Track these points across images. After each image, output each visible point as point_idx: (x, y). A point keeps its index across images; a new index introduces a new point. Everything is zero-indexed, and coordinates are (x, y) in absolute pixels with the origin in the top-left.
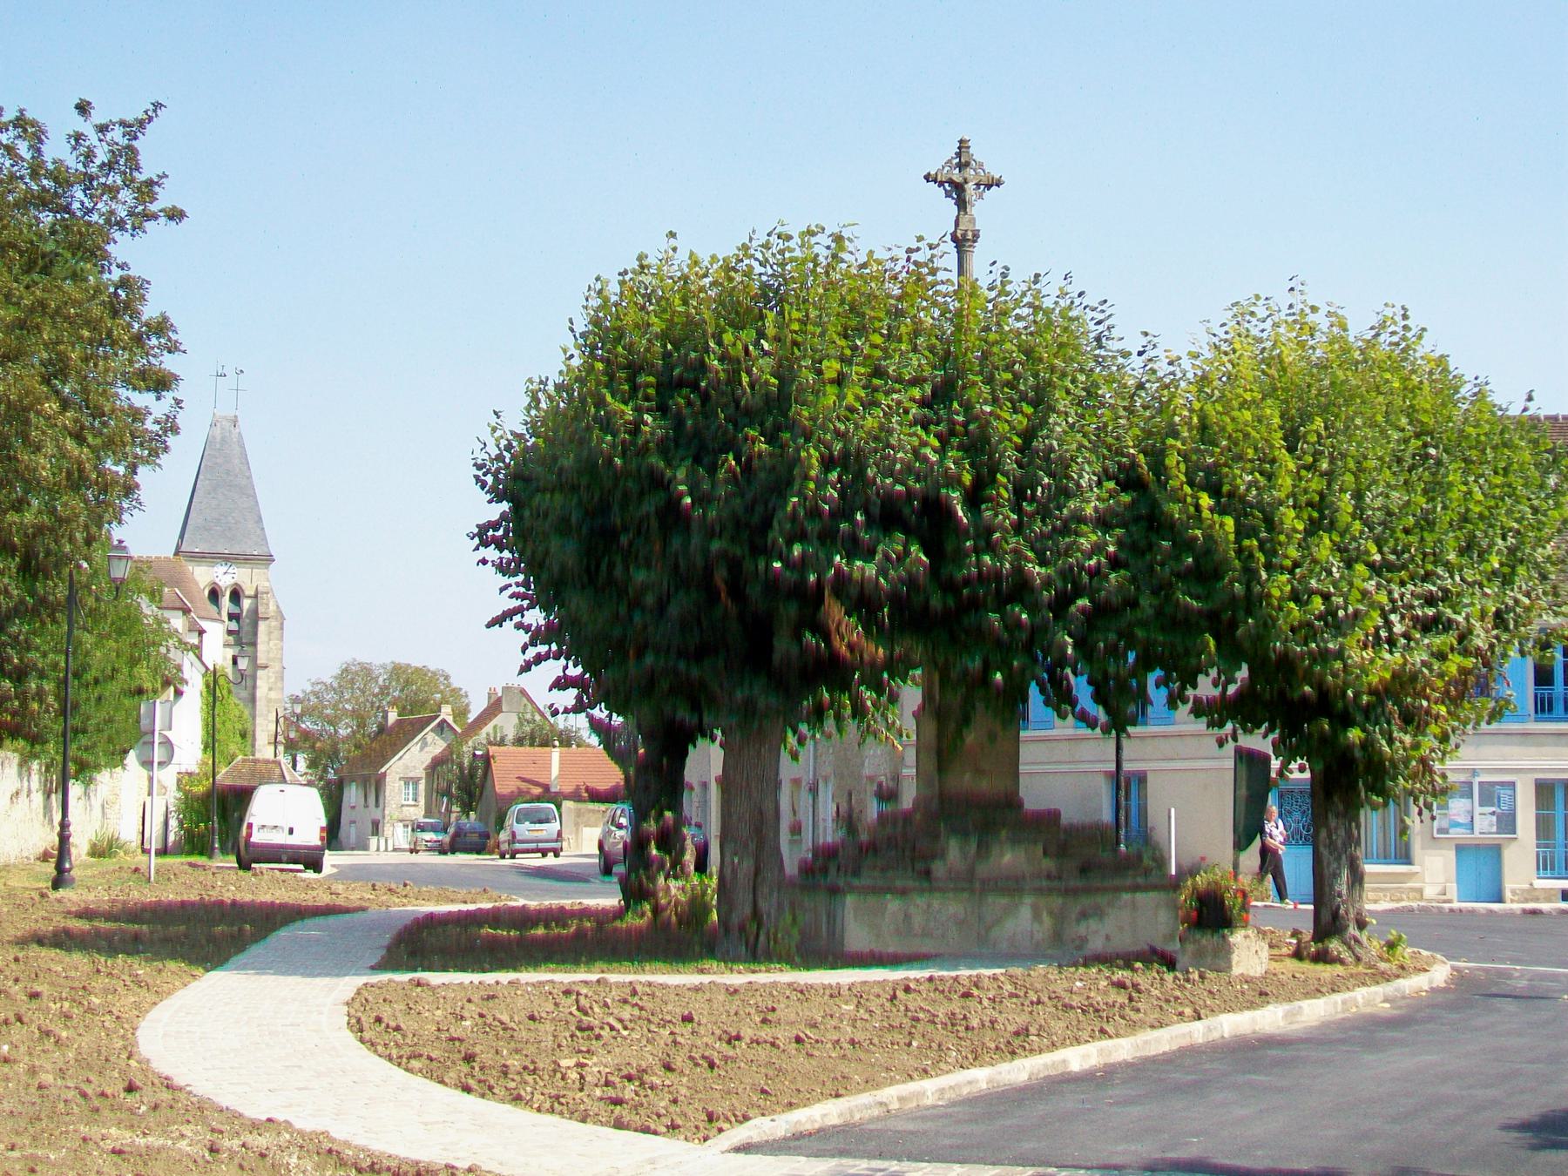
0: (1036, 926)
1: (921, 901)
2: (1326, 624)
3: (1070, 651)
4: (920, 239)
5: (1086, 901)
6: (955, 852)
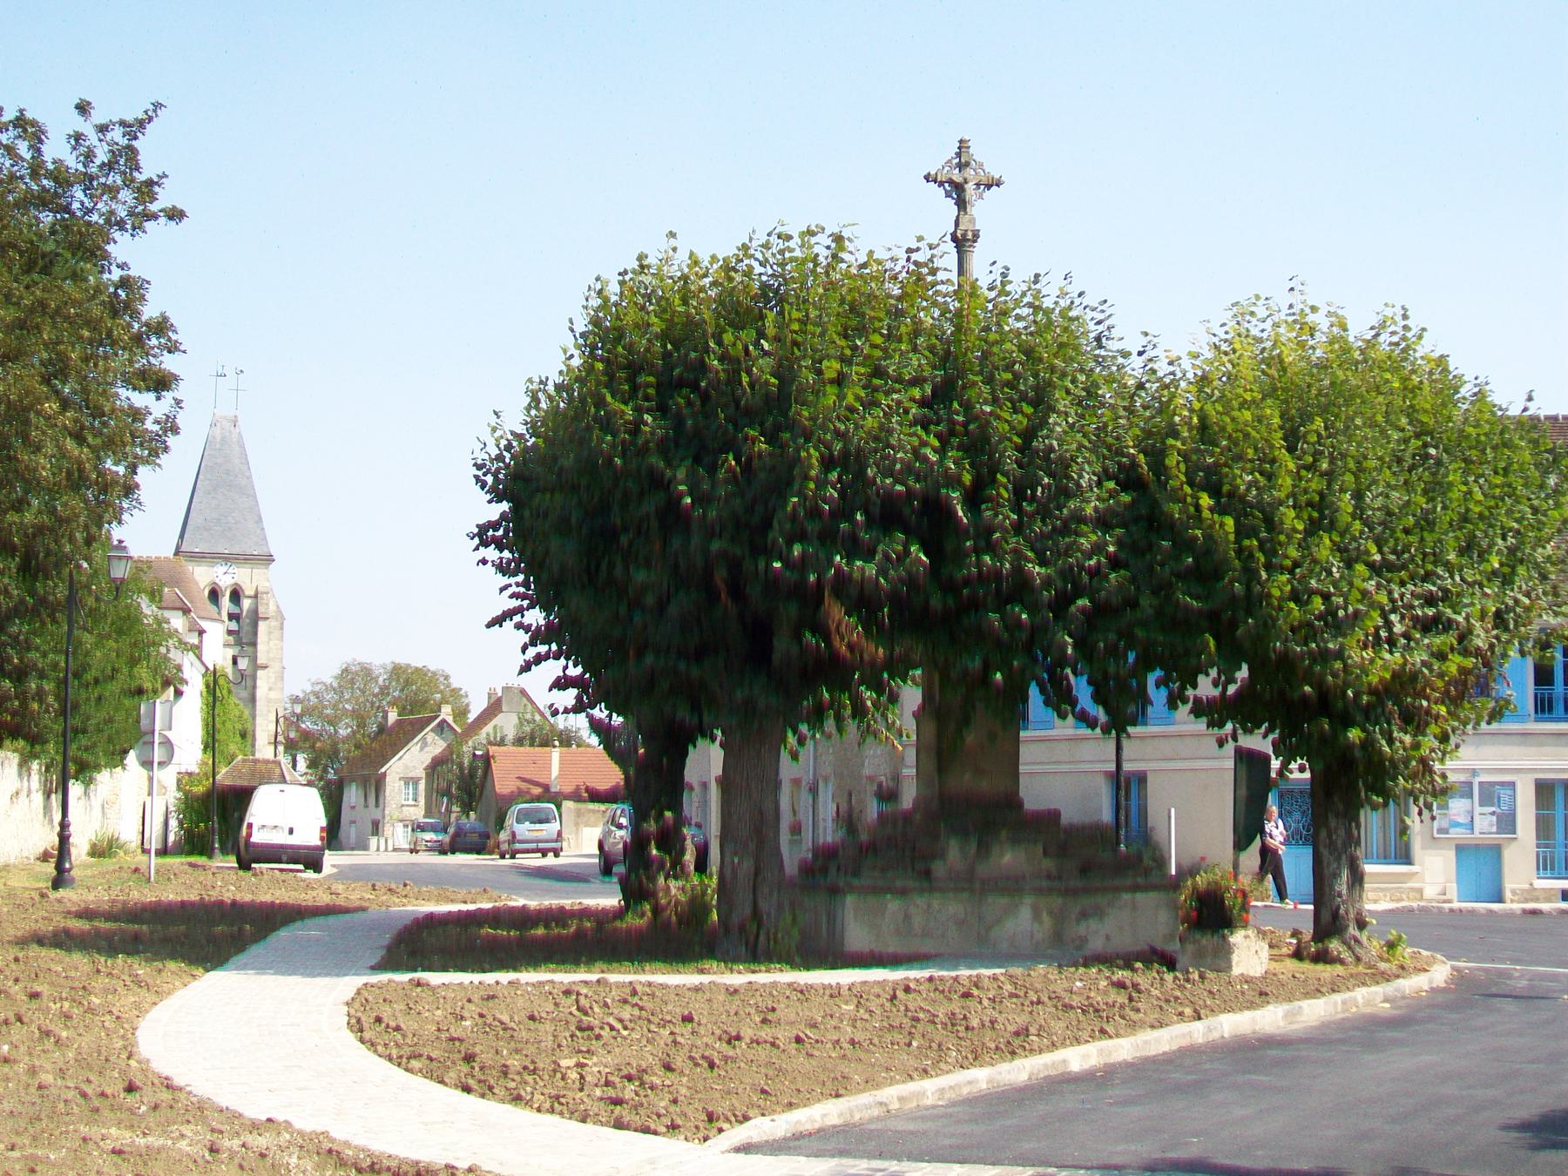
0: (1036, 926)
1: (920, 900)
2: (1326, 624)
3: (1070, 651)
4: (920, 239)
5: (1086, 901)
6: (955, 853)
